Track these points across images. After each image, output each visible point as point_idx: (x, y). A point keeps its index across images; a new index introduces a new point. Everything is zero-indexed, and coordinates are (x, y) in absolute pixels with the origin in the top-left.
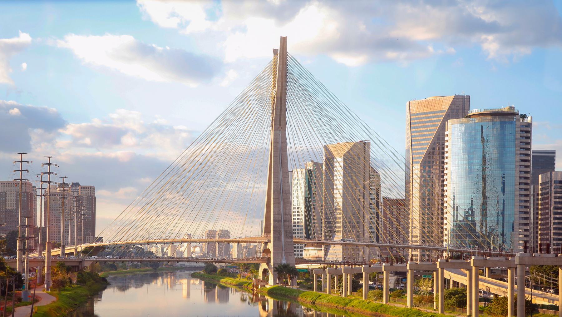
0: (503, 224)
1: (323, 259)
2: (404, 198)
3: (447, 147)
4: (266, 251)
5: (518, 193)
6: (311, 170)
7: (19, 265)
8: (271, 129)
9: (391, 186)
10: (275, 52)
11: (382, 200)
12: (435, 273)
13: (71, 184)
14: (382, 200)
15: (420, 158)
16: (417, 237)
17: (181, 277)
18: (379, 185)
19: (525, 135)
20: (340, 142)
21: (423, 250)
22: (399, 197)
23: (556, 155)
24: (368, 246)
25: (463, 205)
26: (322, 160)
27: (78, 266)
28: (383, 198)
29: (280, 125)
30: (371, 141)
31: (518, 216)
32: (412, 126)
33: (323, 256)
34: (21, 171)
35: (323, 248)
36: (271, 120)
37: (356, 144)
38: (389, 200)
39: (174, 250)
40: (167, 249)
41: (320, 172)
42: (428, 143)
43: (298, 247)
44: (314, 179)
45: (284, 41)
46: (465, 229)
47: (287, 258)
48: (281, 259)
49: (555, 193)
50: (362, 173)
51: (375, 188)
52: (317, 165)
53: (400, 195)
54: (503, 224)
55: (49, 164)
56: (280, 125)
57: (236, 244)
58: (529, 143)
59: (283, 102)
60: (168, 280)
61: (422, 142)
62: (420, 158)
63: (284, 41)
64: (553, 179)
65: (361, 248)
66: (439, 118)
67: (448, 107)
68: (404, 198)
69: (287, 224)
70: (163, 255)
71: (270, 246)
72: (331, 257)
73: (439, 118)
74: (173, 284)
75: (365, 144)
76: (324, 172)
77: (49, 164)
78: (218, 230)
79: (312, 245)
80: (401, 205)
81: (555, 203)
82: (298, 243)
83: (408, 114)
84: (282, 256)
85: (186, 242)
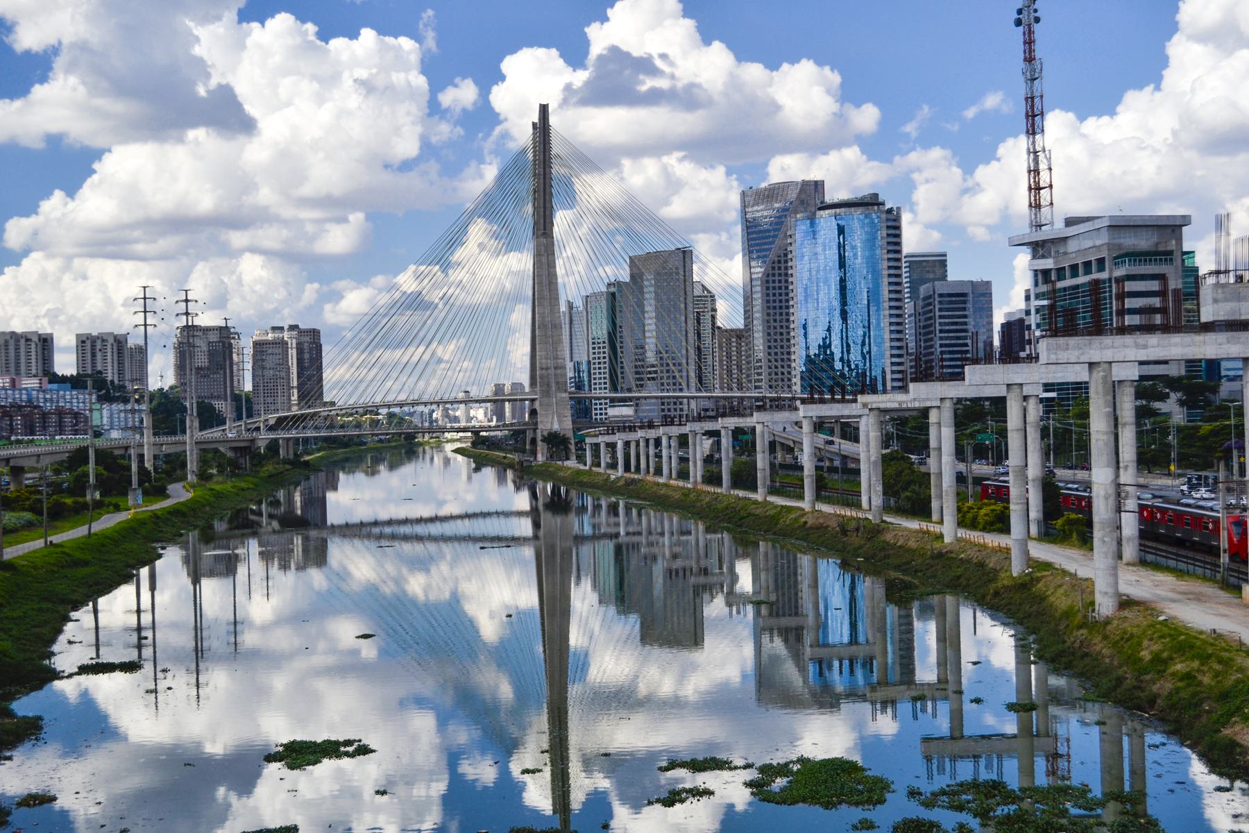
2: (742, 327)
5: (887, 312)
12: (484, 434)
13: (286, 327)
19: (893, 232)
21: (495, 401)
23: (948, 258)
24: (693, 398)
27: (249, 447)
39: (446, 415)
47: (560, 422)
49: (940, 310)
50: (682, 293)
53: (739, 323)
55: (187, 301)
58: (899, 244)
64: (937, 292)
65: (685, 401)
68: (742, 327)
69: (559, 371)
80: (740, 336)
81: (940, 324)
82: (599, 399)
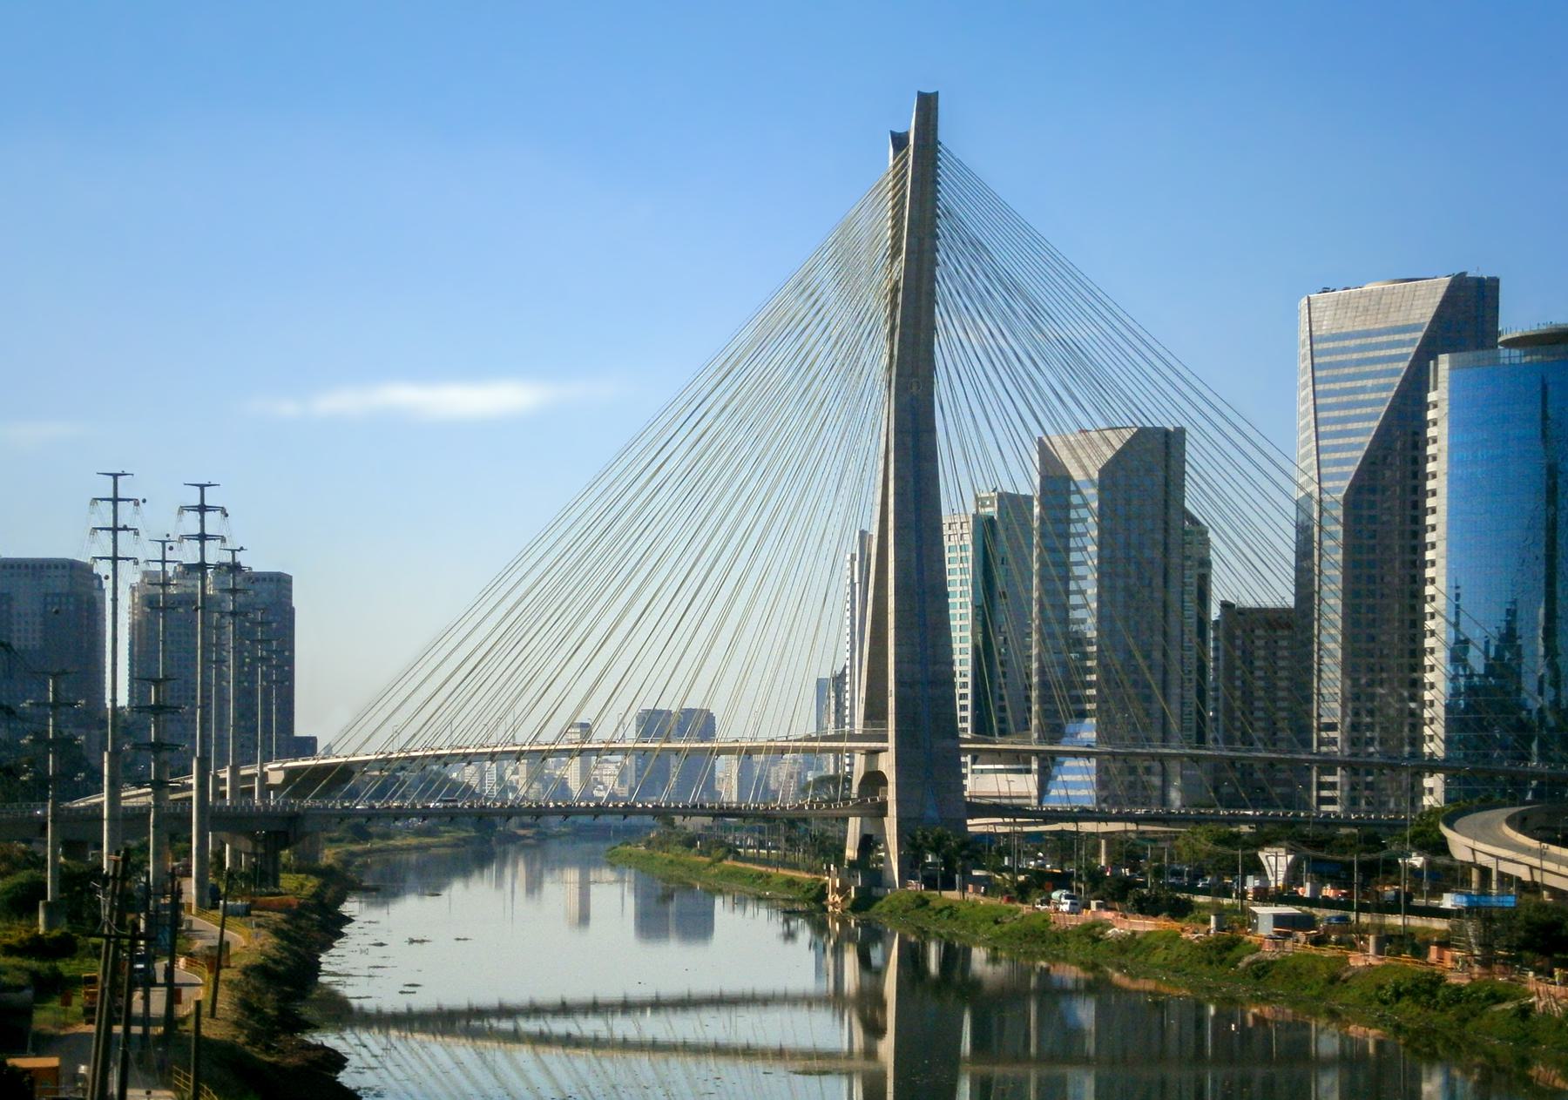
0: (479, 624)
1: (1034, 802)
3: (1435, 441)
4: (874, 780)
6: (991, 520)
7: (110, 830)
8: (885, 392)
9: (1250, 569)
10: (899, 141)
11: (1215, 613)
14: (1215, 613)
15: (1342, 476)
16: (1331, 727)
17: (563, 863)
18: (1206, 563)
20: (1088, 426)
22: (1268, 602)
25: (1483, 630)
26: (1028, 484)
28: (1226, 606)
30: (1188, 428)
32: (1318, 374)
33: (1035, 792)
34: (115, 530)
35: (1035, 766)
36: (885, 360)
37: (1143, 433)
38: (1243, 612)
40: (515, 772)
41: (1026, 523)
42: (1370, 429)
44: (1004, 546)
45: (928, 106)
46: (1485, 706)
51: (1196, 572)
52: (1012, 503)
53: (1279, 593)
54: (479, 624)
55: (202, 509)
57: (831, 756)
60: (517, 874)
61: (1339, 427)
62: (1342, 476)
63: (928, 106)
66: (1405, 350)
67: (1428, 319)
68: (1291, 601)
70: (504, 791)
71: (887, 764)
72: (1057, 797)
73: (1405, 350)
74: (534, 886)
76: (1036, 524)
77: (202, 509)
78: (674, 709)
79: (997, 756)
83: (1304, 335)
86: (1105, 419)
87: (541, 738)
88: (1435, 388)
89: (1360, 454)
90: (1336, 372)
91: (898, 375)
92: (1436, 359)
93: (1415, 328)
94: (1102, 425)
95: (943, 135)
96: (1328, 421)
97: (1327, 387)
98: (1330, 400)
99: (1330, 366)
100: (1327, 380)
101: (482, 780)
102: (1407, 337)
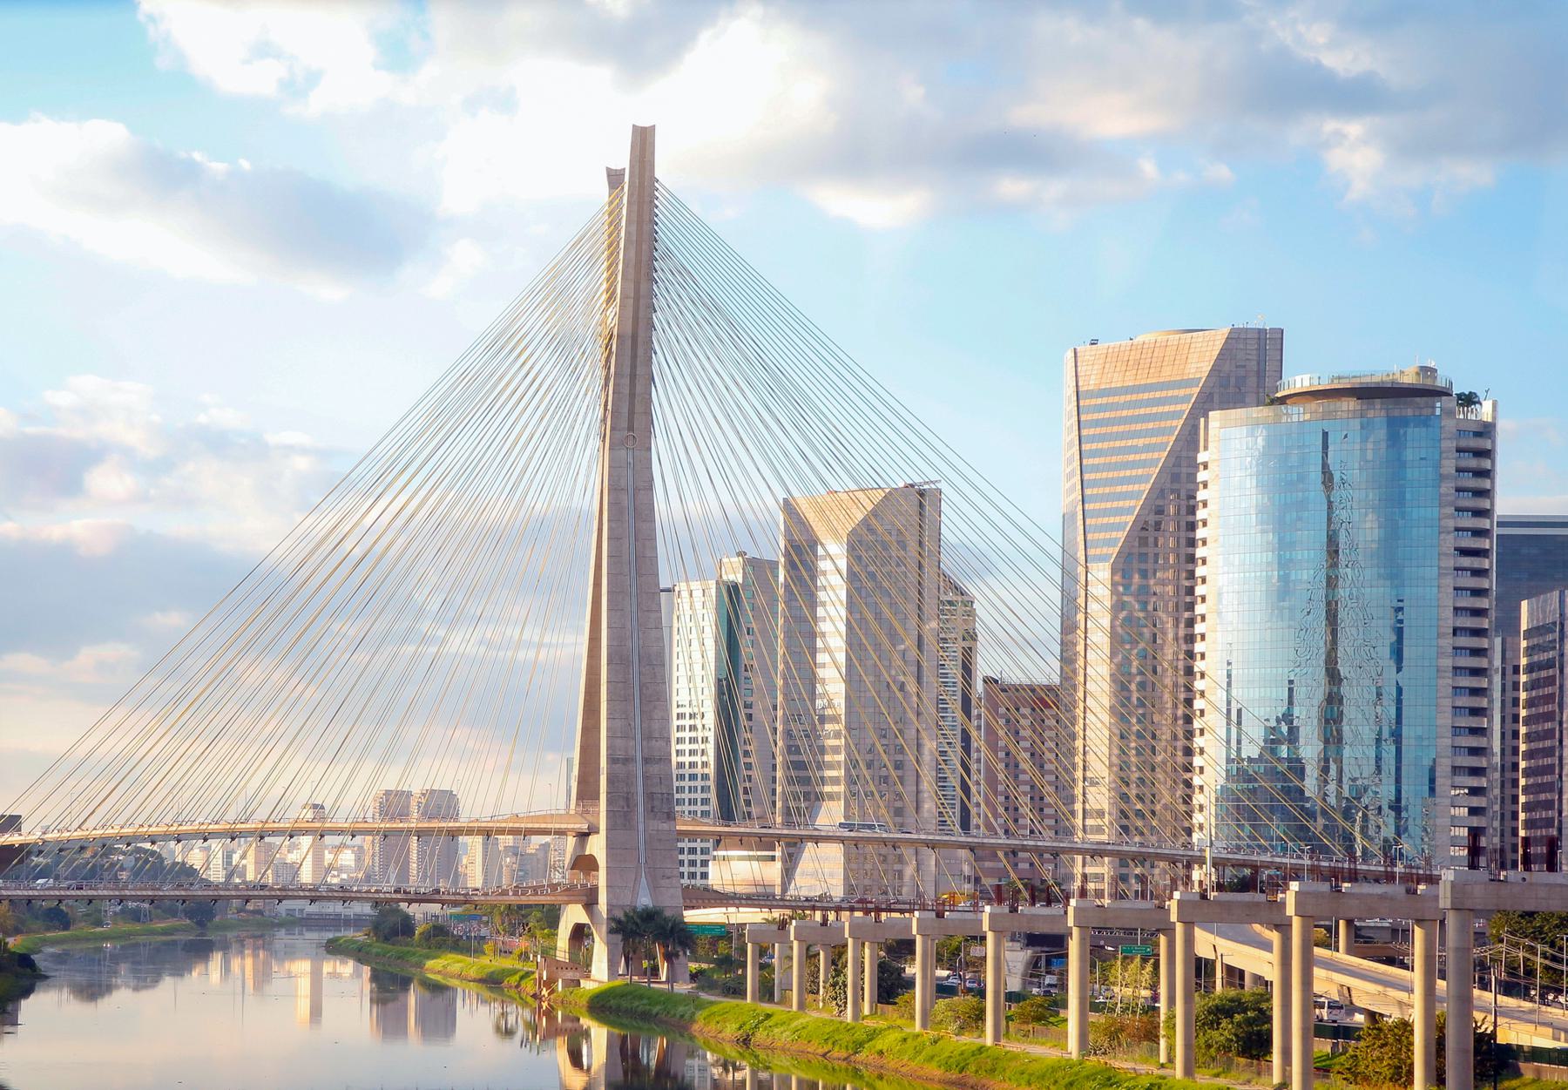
1: (778, 891)
2: (1056, 680)
4: (584, 863)
6: (735, 586)
8: (598, 443)
10: (614, 178)
11: (979, 687)
14: (979, 687)
15: (1110, 543)
16: (1100, 814)
17: (291, 954)
22: (1041, 680)
24: (932, 845)
26: (774, 549)
29: (631, 428)
30: (943, 486)
31: (1448, 742)
33: (778, 881)
35: (778, 853)
43: (692, 851)
44: (748, 617)
45: (643, 141)
46: (1268, 789)
48: (635, 893)
51: (957, 648)
52: (758, 568)
53: (1045, 672)
56: (631, 428)
58: (1486, 493)
59: (640, 352)
60: (244, 964)
63: (643, 141)
68: (1056, 680)
70: (230, 876)
71: (597, 847)
72: (805, 884)
74: (263, 977)
75: (922, 494)
78: (416, 790)
79: (742, 841)
80: (1046, 706)
82: (693, 836)
83: (1071, 391)
84: (637, 880)
85: (306, 832)
86: (856, 483)
87: (90, 824)
88: (1206, 448)
89: (1131, 519)
90: (1104, 430)
91: (612, 429)
92: (1206, 417)
93: (1189, 383)
94: (854, 487)
95: (661, 171)
96: (1095, 483)
97: (1094, 446)
98: (1097, 461)
99: (1097, 423)
100: (1093, 439)
101: (208, 862)
102: (1182, 392)
